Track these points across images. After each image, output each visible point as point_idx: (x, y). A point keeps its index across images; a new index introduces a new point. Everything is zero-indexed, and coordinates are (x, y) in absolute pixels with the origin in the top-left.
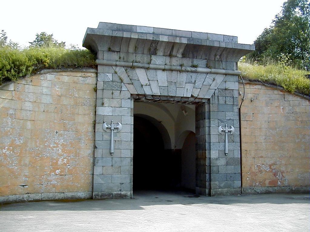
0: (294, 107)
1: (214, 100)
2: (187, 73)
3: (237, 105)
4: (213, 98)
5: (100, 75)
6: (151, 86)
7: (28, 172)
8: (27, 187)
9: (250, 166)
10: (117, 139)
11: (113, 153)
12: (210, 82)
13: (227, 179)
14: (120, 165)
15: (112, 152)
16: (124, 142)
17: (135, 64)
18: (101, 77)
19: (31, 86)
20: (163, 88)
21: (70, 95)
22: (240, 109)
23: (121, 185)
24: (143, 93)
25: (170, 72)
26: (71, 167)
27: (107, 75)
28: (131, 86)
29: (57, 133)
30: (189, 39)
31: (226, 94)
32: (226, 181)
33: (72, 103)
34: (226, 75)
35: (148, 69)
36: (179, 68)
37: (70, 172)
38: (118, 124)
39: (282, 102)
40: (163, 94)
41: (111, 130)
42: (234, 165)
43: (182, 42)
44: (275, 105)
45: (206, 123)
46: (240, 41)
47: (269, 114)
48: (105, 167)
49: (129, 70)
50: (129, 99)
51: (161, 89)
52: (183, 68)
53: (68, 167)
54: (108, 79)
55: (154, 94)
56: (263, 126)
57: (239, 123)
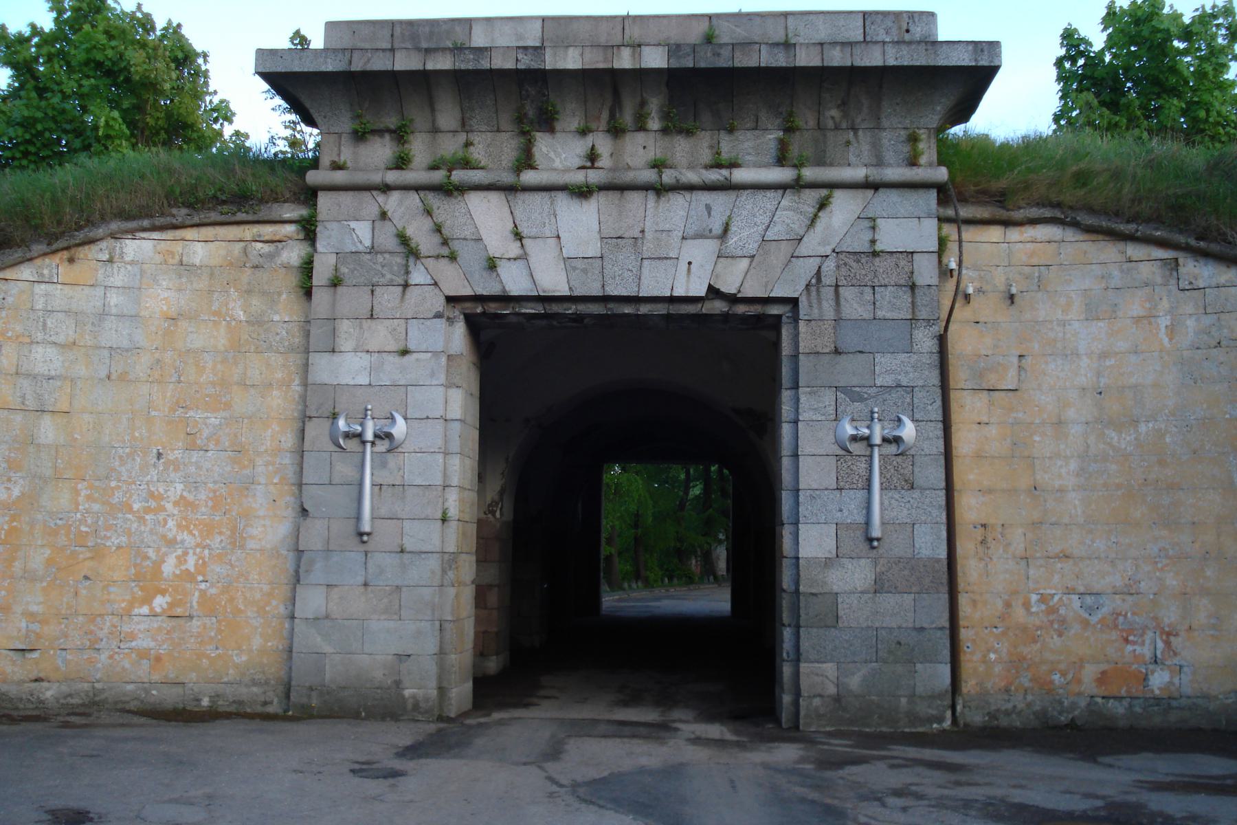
0: (1223, 316)
1: (814, 301)
3: (929, 322)
6: (532, 260)
7: (41, 599)
8: (35, 655)
10: (385, 477)
11: (878, 540)
13: (880, 653)
14: (399, 582)
17: (459, 176)
19: (59, 286)
21: (216, 313)
22: (942, 340)
23: (400, 661)
25: (613, 196)
26: (212, 586)
27: (352, 227)
29: (159, 455)
30: (674, 49)
31: (875, 276)
32: (874, 664)
33: (223, 343)
36: (649, 176)
37: (209, 606)
39: (1165, 299)
41: (364, 443)
42: (914, 589)
44: (1135, 314)
45: (784, 407)
46: (944, 33)
47: (1104, 355)
48: (336, 589)
49: (433, 199)
50: (438, 316)
52: (668, 177)
53: (203, 586)
54: (354, 244)
55: (544, 292)
56: (1071, 413)
57: (939, 403)
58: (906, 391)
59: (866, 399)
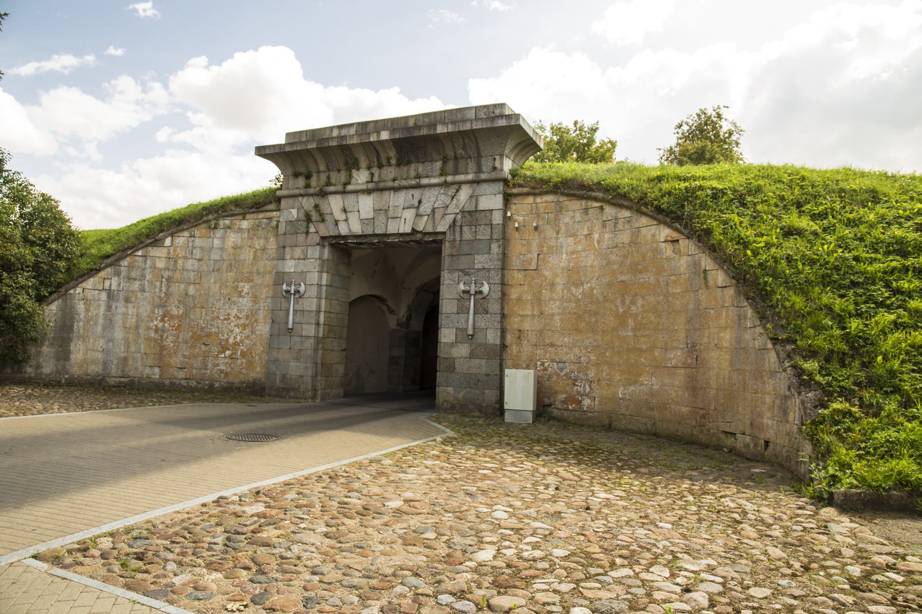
10: (298, 307)
29: (229, 299)
38: (300, 284)
40: (366, 233)
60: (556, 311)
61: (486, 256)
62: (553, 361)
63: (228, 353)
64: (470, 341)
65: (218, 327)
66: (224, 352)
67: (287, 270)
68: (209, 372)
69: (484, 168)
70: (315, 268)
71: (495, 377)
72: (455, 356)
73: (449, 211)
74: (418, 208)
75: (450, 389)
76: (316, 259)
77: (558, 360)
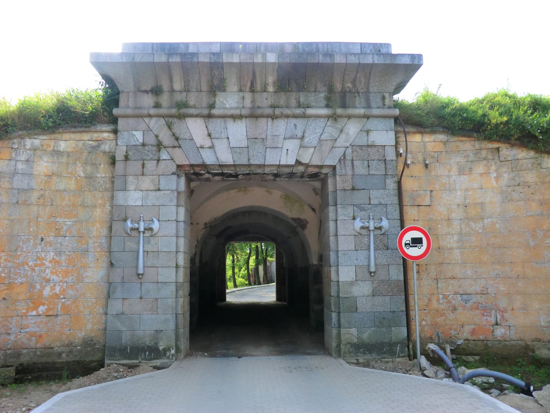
1: (343, 167)
2: (286, 120)
4: (342, 163)
5: (122, 134)
9: (429, 296)
10: (149, 248)
11: (142, 275)
12: (335, 134)
15: (141, 272)
16: (164, 254)
18: (123, 138)
20: (237, 150)
24: (199, 162)
28: (177, 151)
29: (42, 240)
31: (369, 156)
34: (368, 118)
35: (210, 116)
36: (269, 111)
38: (153, 221)
40: (238, 162)
43: (267, 61)
45: (330, 214)
51: (236, 152)
53: (63, 300)
54: (135, 141)
55: (222, 162)
56: (454, 215)
57: (398, 211)
58: (383, 206)
59: (367, 210)
60: (455, 245)
61: (382, 191)
62: (456, 293)
63: (42, 309)
64: (372, 279)
65: (26, 276)
66: (36, 308)
67: (131, 203)
68: (12, 338)
69: (373, 104)
70: (171, 201)
71: (401, 313)
72: (355, 295)
73: (338, 144)
74: (302, 138)
75: (354, 331)
76: (172, 191)
77: (462, 292)
